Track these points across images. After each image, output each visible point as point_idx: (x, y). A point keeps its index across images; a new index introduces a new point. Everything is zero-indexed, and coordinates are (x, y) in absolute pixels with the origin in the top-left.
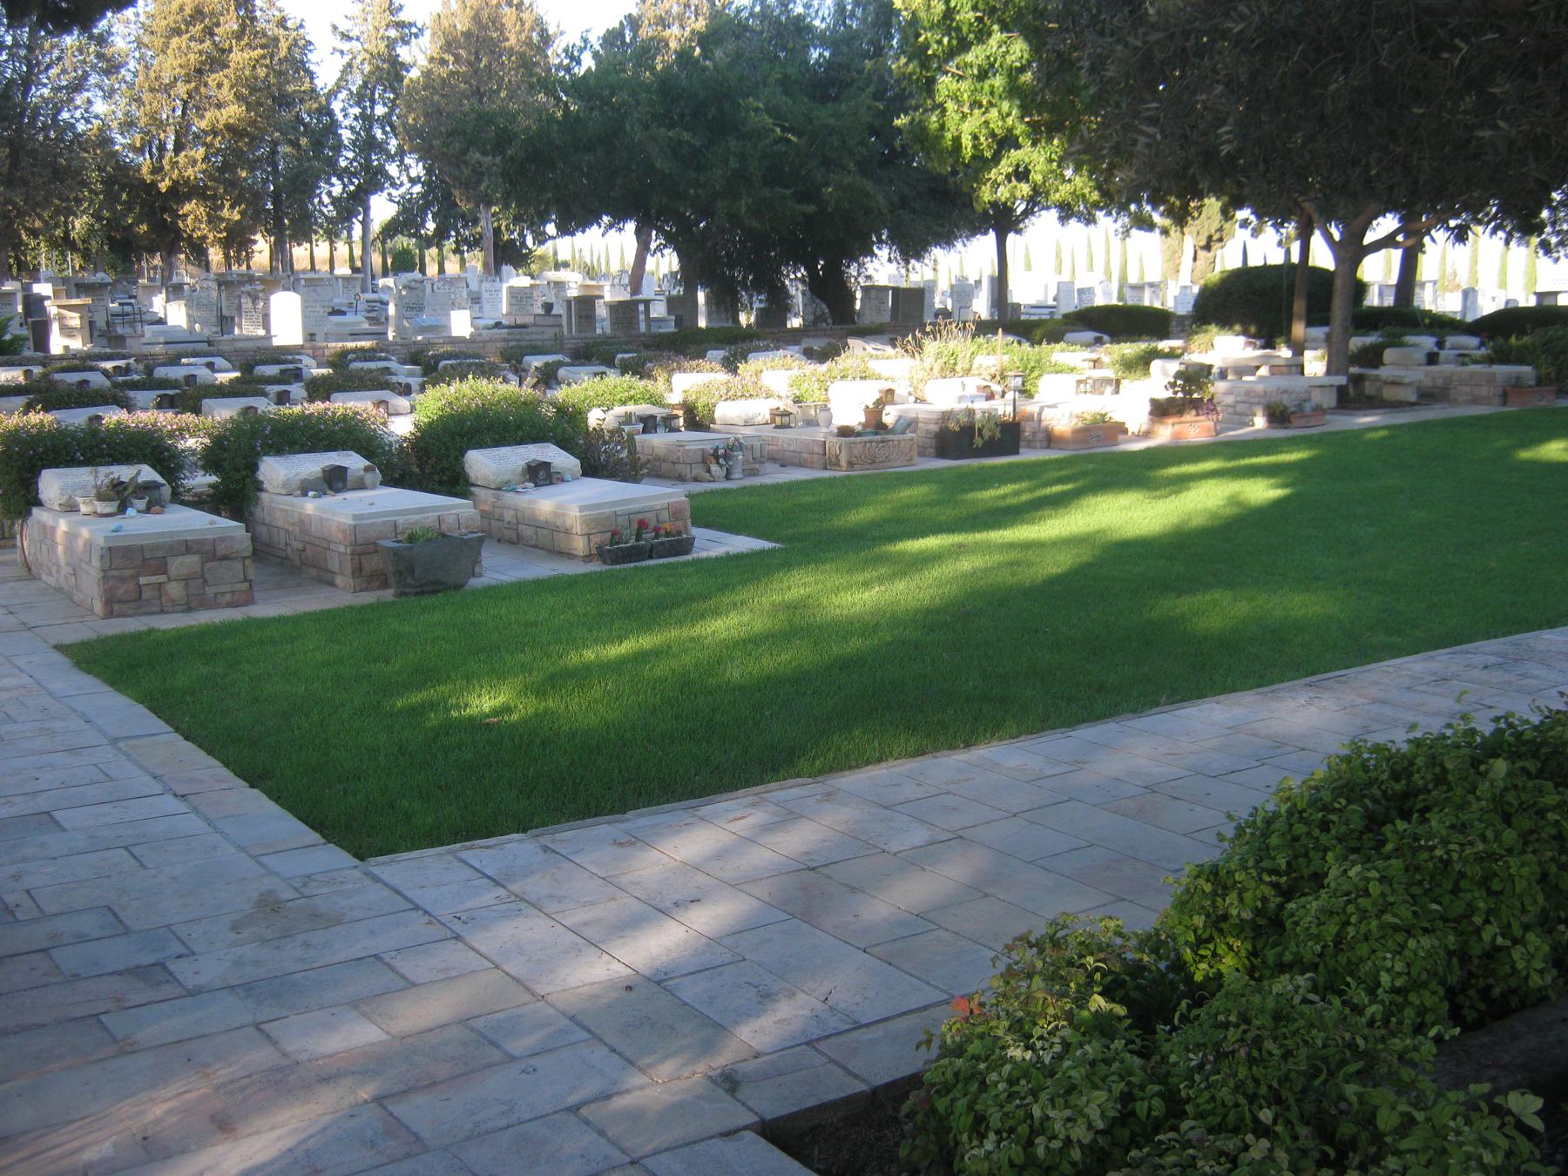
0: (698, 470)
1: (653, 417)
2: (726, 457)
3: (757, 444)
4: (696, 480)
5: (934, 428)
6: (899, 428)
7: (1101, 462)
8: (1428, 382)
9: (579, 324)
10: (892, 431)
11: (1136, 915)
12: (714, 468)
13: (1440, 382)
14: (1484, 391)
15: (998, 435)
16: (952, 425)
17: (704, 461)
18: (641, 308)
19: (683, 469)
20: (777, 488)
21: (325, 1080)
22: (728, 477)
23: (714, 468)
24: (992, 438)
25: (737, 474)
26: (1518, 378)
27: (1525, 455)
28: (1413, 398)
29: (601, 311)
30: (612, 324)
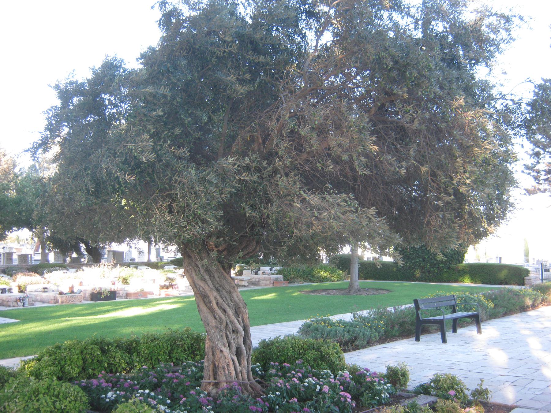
0: (14, 304)
1: (5, 289)
2: (23, 300)
3: (34, 296)
4: (14, 306)
5: (90, 293)
6: (78, 292)
7: (141, 299)
8: (254, 280)
9: (7, 262)
10: (76, 293)
11: (109, 339)
12: (19, 303)
13: (257, 280)
14: (268, 282)
15: (109, 294)
16: (95, 291)
17: (16, 301)
18: (30, 256)
19: (10, 304)
20: (40, 308)
21: (22, 347)
22: (23, 305)
23: (19, 303)
24: (107, 295)
25: (26, 305)
26: (277, 279)
27: (420, 359)
28: (247, 284)
29: (15, 257)
30: (19, 261)
